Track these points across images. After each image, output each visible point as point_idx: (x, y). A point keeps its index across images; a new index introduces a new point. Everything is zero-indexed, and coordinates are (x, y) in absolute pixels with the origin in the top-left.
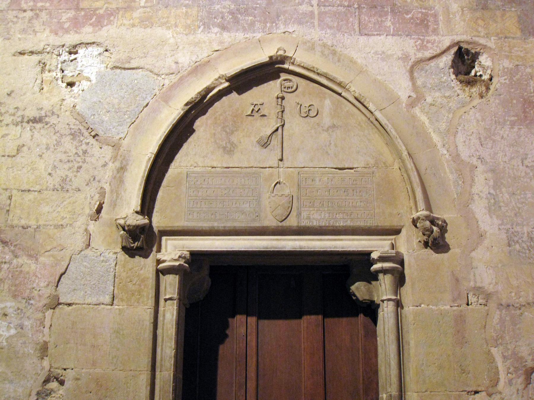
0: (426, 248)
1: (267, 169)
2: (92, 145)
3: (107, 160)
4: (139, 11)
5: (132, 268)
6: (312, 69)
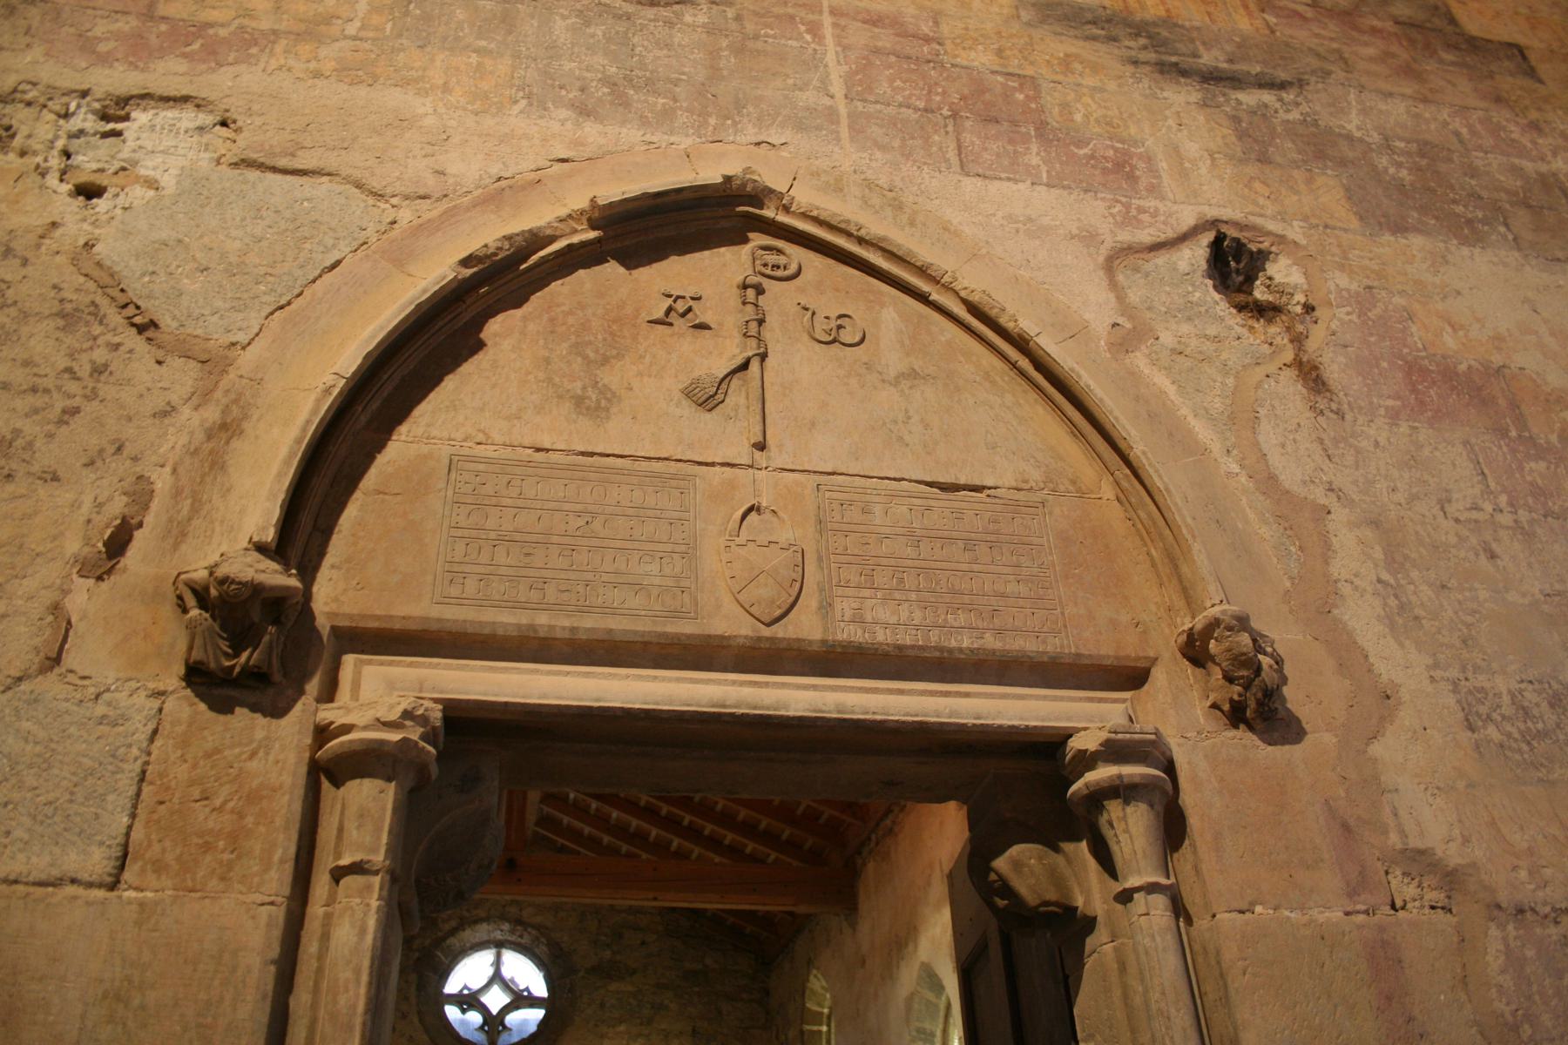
0: (1236, 727)
1: (717, 468)
2: (131, 351)
3: (174, 399)
4: (337, 45)
5: (217, 751)
6: (843, 226)
